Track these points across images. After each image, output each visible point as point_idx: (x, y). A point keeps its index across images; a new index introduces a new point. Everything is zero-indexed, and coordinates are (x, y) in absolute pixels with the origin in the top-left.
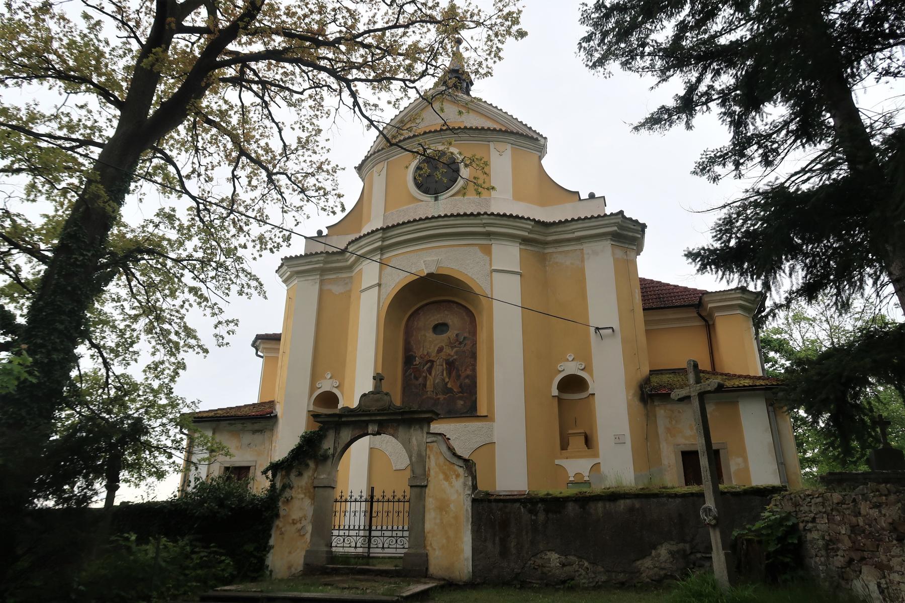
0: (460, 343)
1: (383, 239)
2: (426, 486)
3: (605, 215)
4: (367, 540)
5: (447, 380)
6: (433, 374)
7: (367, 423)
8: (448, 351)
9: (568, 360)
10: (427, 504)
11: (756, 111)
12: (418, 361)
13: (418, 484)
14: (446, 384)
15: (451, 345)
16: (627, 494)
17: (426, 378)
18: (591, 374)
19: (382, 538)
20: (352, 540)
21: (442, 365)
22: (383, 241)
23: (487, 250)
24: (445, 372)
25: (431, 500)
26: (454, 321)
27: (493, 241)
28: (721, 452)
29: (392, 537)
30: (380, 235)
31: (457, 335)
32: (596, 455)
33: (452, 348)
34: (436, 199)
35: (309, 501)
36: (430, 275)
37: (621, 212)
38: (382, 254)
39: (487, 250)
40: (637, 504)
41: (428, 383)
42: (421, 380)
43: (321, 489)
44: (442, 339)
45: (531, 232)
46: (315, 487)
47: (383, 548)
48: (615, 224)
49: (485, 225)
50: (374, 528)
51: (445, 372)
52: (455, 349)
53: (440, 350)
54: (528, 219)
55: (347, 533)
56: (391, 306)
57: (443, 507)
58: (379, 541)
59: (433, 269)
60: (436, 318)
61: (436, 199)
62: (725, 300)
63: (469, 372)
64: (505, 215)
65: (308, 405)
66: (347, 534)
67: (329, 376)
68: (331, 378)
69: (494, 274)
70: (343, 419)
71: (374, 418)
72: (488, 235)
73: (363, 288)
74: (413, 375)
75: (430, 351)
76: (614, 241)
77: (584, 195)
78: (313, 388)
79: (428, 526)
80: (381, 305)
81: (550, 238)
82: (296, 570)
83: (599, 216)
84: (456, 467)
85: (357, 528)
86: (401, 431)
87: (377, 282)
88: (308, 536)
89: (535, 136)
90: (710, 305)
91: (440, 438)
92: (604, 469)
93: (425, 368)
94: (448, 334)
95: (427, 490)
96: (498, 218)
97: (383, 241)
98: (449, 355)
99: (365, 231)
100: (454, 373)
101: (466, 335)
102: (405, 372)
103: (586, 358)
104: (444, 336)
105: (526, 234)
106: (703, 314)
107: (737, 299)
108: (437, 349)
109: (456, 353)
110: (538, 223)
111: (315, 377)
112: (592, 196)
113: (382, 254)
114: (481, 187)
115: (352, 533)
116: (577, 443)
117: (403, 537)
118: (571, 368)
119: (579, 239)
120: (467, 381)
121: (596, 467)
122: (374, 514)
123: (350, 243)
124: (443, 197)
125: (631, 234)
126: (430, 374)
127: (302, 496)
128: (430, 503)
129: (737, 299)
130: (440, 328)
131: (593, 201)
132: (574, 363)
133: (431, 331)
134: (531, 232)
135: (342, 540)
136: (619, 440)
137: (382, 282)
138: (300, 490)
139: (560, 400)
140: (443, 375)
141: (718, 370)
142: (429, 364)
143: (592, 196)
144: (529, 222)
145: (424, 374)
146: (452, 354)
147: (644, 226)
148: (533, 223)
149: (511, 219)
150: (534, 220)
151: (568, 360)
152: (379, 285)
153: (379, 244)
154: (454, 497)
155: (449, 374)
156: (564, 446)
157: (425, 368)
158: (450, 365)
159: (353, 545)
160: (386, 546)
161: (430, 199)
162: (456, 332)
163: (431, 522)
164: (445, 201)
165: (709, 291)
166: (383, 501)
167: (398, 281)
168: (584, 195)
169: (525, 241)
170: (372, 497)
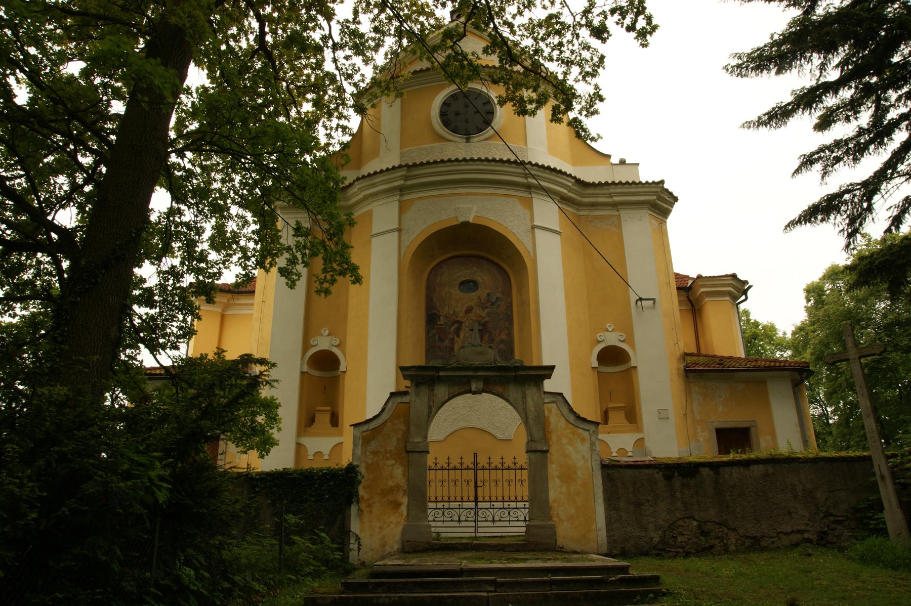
0: (493, 304)
1: (406, 178)
2: (547, 451)
4: (473, 513)
6: (462, 336)
7: (468, 380)
9: (607, 330)
10: (549, 470)
12: (442, 321)
13: (539, 448)
15: (482, 306)
16: (762, 460)
17: (453, 340)
19: (491, 510)
20: (454, 513)
22: (405, 180)
25: (554, 466)
26: (485, 278)
27: (533, 195)
28: (752, 430)
29: (503, 508)
30: (404, 173)
31: (488, 295)
32: (639, 429)
33: (484, 308)
34: (468, 140)
35: (402, 468)
37: (662, 182)
38: (401, 195)
39: (529, 205)
40: (770, 469)
42: (447, 342)
43: (416, 455)
44: (471, 298)
46: (408, 452)
48: (655, 193)
50: (480, 499)
52: (486, 311)
53: (469, 310)
54: (570, 176)
55: (446, 505)
56: (415, 254)
57: (568, 476)
58: (488, 513)
61: (468, 140)
62: (715, 286)
63: (504, 337)
64: (549, 168)
65: (302, 365)
67: (327, 332)
68: (329, 335)
69: (536, 230)
70: (441, 374)
71: (480, 373)
73: (374, 232)
74: (437, 336)
76: (651, 211)
77: (615, 160)
78: (306, 346)
79: (552, 495)
80: (402, 254)
81: (586, 200)
82: (392, 548)
83: (634, 183)
84: (581, 431)
85: (459, 499)
86: (514, 392)
87: (396, 226)
88: (404, 509)
91: (560, 398)
92: (648, 443)
93: (452, 329)
94: (478, 293)
95: (549, 455)
96: (541, 170)
97: (405, 180)
98: (480, 316)
99: (365, 171)
100: (486, 337)
104: (473, 295)
105: (565, 191)
107: (729, 285)
108: (464, 309)
109: (489, 314)
110: (579, 182)
111: (308, 333)
112: (622, 162)
113: (401, 195)
117: (516, 508)
118: (612, 339)
119: (615, 205)
121: (640, 442)
122: (479, 484)
123: (358, 179)
124: (476, 139)
125: (665, 206)
126: (458, 336)
127: (393, 462)
128: (553, 469)
129: (729, 285)
130: (469, 285)
131: (623, 167)
132: (613, 334)
133: (457, 288)
134: (570, 189)
135: (441, 513)
136: (663, 416)
137: (403, 226)
138: (388, 455)
141: (703, 352)
142: (456, 325)
143: (622, 162)
144: (569, 179)
145: (451, 336)
146: (484, 315)
147: (676, 199)
148: (573, 181)
149: (554, 173)
150: (575, 178)
151: (607, 330)
152: (399, 230)
154: (581, 463)
157: (452, 329)
159: (490, 518)
160: (497, 518)
161: (459, 140)
162: (487, 291)
163: (555, 491)
164: (478, 144)
165: (704, 276)
167: (424, 227)
168: (615, 160)
169: (564, 199)
170: (476, 463)
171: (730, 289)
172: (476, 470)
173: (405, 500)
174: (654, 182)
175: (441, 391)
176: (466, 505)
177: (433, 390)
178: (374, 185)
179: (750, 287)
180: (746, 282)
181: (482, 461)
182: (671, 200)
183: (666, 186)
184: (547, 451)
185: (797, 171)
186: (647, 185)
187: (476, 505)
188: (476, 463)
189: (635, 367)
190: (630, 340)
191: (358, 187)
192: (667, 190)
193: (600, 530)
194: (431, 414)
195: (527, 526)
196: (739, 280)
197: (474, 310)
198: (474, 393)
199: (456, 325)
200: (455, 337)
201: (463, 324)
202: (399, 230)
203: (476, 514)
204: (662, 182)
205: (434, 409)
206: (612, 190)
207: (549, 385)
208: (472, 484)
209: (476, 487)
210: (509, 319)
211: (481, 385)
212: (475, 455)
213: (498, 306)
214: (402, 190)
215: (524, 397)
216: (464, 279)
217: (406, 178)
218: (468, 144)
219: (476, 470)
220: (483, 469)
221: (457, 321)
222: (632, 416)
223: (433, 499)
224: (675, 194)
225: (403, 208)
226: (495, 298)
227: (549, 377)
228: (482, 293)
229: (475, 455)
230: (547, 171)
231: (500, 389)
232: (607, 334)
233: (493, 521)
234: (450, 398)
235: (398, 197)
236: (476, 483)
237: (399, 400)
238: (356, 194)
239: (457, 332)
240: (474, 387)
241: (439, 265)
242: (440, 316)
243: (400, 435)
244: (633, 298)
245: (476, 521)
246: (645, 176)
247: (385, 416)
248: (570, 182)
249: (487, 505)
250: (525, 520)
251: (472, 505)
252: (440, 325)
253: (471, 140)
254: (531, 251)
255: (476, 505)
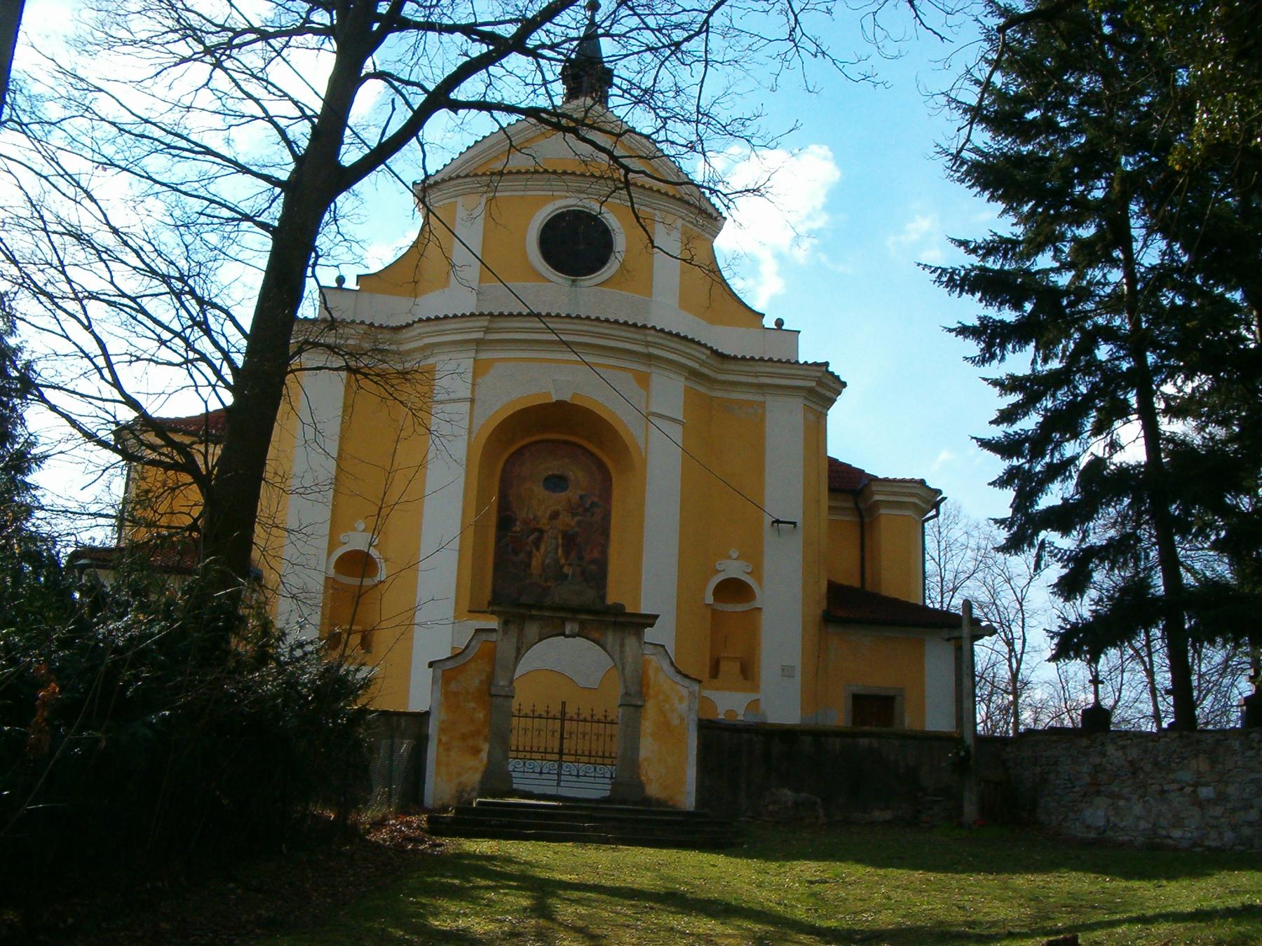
0: (586, 510)
1: (487, 330)
2: (642, 706)
3: (797, 362)
4: (556, 766)
5: (563, 561)
8: (566, 519)
11: (1065, 338)
12: (518, 527)
14: (562, 567)
17: (530, 554)
18: (759, 579)
21: (556, 538)
22: (485, 333)
23: (643, 381)
24: (560, 550)
26: (577, 475)
27: (653, 369)
30: (486, 324)
31: (581, 497)
32: (756, 688)
33: (574, 515)
36: (560, 404)
37: (827, 364)
38: (477, 351)
39: (643, 381)
41: (534, 562)
42: (522, 556)
44: (557, 500)
45: (703, 364)
47: (578, 776)
49: (648, 344)
51: (560, 550)
52: (577, 519)
53: (555, 516)
54: (705, 346)
55: (528, 755)
59: (567, 397)
60: (553, 466)
63: (596, 554)
66: (528, 757)
68: (363, 531)
72: (650, 357)
75: (539, 514)
77: (769, 322)
79: (643, 753)
83: (788, 362)
86: (610, 638)
89: (715, 214)
90: (877, 497)
91: (660, 649)
93: (532, 537)
96: (669, 337)
97: (485, 333)
101: (595, 499)
102: (499, 539)
103: (754, 557)
105: (696, 366)
106: (862, 506)
107: (912, 495)
109: (579, 523)
110: (715, 353)
113: (477, 351)
114: (630, 278)
115: (535, 756)
116: (730, 668)
118: (734, 569)
120: (593, 567)
122: (565, 735)
126: (538, 549)
130: (556, 483)
134: (703, 364)
136: (787, 672)
139: (714, 612)
140: (556, 553)
142: (536, 534)
147: (844, 385)
150: (711, 349)
153: (480, 335)
155: (567, 554)
156: (715, 671)
157: (532, 537)
158: (570, 541)
161: (560, 281)
162: (580, 492)
166: (579, 719)
169: (694, 374)
170: (563, 713)
171: (915, 500)
172: (563, 720)
173: (486, 747)
174: (815, 364)
175: (532, 630)
176: (549, 757)
177: (522, 630)
178: (442, 333)
179: (944, 499)
180: (939, 492)
181: (571, 711)
182: (835, 386)
183: (830, 369)
184: (642, 706)
185: (985, 379)
186: (805, 367)
187: (561, 758)
188: (563, 713)
189: (760, 609)
190: (757, 572)
191: (419, 331)
192: (832, 373)
193: (689, 793)
194: (519, 655)
195: (612, 784)
196: (928, 488)
197: (561, 517)
198: (567, 636)
199: (536, 534)
200: (534, 551)
201: (546, 535)
202: (472, 401)
203: (560, 766)
204: (827, 364)
205: (522, 652)
206: (760, 368)
207: (649, 634)
208: (558, 735)
209: (562, 738)
210: (605, 531)
211: (576, 628)
212: (564, 704)
213: (593, 514)
214: (478, 342)
215: (622, 645)
216: (550, 473)
217: (487, 330)
218: (573, 289)
219: (563, 720)
220: (571, 719)
221: (535, 530)
222: (748, 672)
223: (514, 748)
224: (843, 379)
225: (480, 369)
226: (589, 502)
227: (651, 625)
228: (572, 494)
229: (564, 704)
230: (675, 339)
231: (596, 635)
232: (729, 562)
233: (578, 776)
234: (540, 640)
235: (473, 354)
236: (562, 734)
237: (484, 637)
238: (413, 339)
239: (537, 544)
240: (568, 629)
241: (519, 453)
242: (516, 520)
243: (483, 677)
244: (768, 520)
245: (559, 774)
246: (807, 353)
247: (471, 653)
248: (704, 354)
249: (572, 759)
250: (611, 778)
251: (556, 757)
252: (516, 532)
253: (578, 283)
254: (642, 446)
255: (561, 758)
